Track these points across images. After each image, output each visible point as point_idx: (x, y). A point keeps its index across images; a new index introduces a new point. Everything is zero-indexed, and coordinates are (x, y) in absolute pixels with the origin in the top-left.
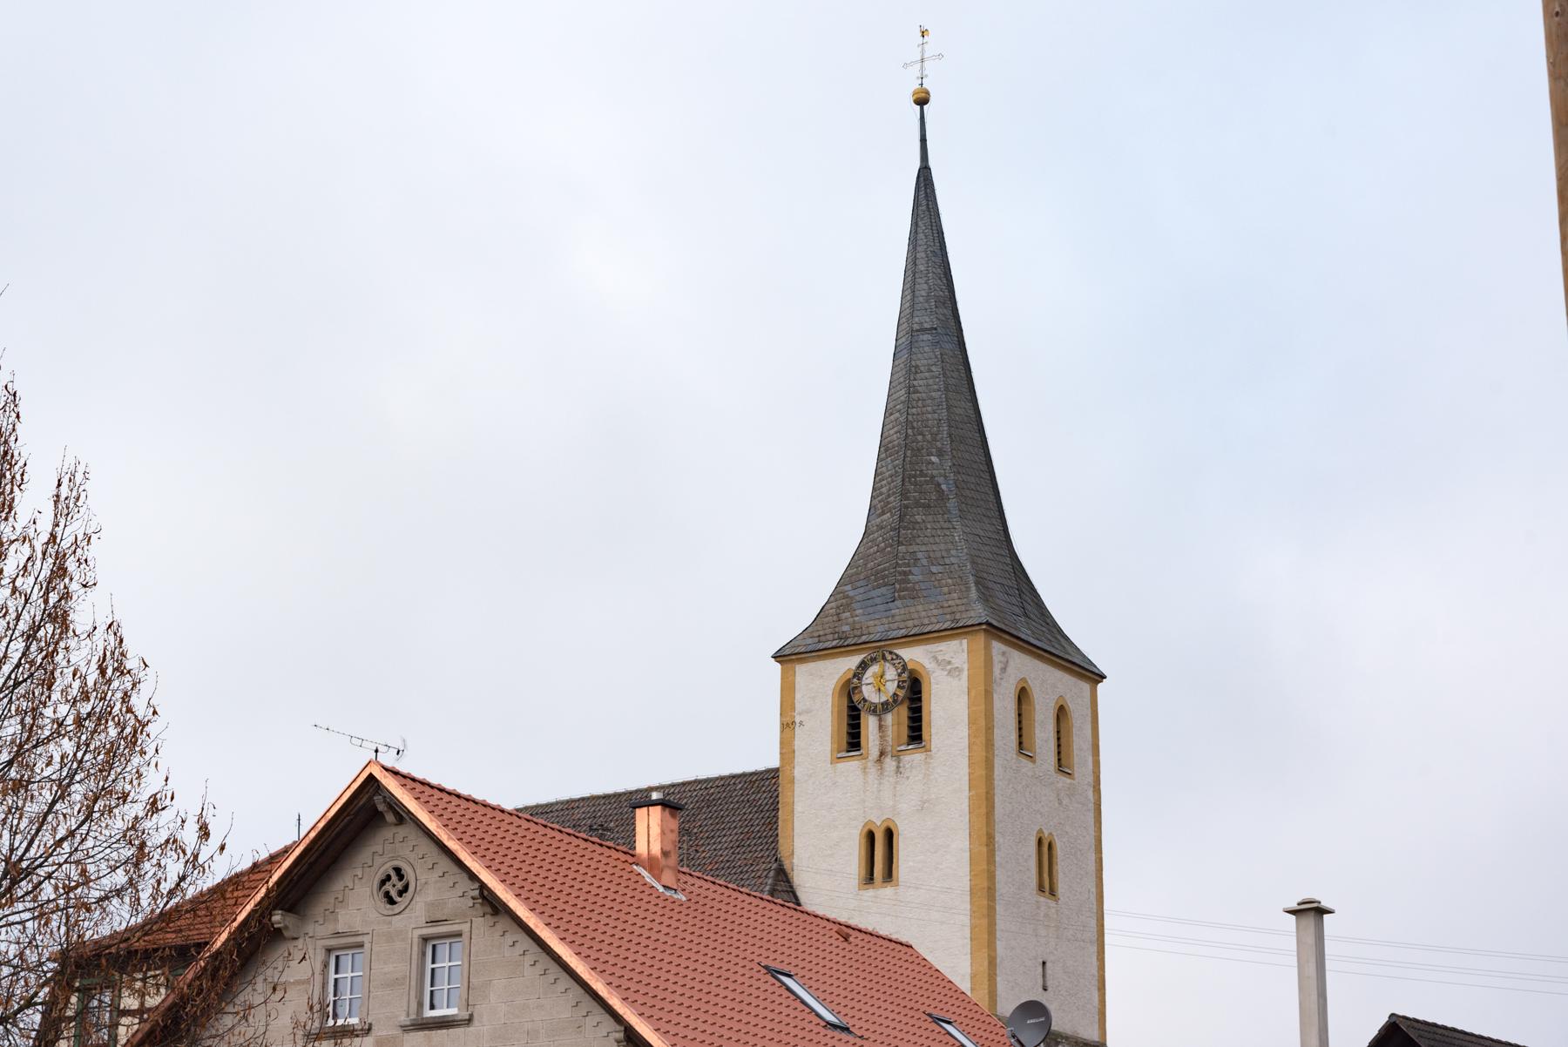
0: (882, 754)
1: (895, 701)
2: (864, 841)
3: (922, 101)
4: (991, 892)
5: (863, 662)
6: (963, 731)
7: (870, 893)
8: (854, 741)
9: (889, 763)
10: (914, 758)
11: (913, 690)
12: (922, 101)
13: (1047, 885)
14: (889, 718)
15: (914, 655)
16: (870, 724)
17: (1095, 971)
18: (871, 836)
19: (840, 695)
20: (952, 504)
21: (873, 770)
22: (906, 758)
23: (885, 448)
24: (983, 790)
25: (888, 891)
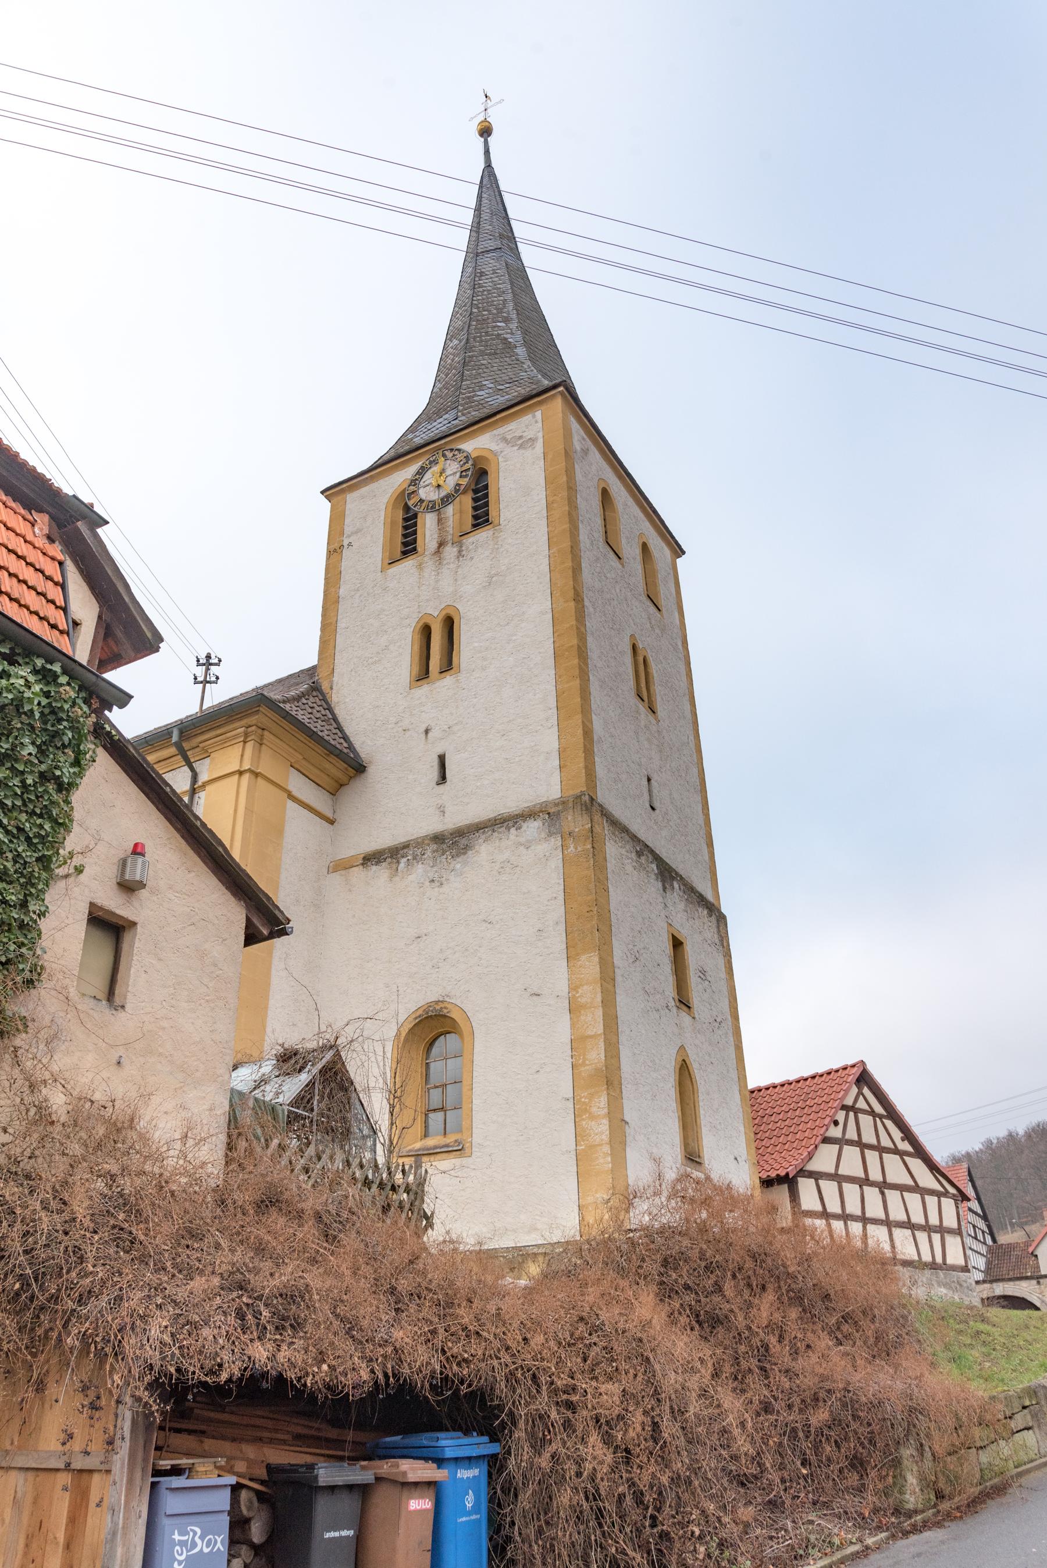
0: (441, 544)
1: (456, 491)
2: (417, 637)
3: (486, 131)
4: (582, 653)
5: (422, 468)
6: (539, 496)
7: (425, 689)
8: (409, 546)
9: (450, 551)
10: (483, 535)
11: (479, 486)
12: (486, 131)
13: (645, 694)
14: (450, 510)
15: (474, 445)
16: (428, 526)
17: (701, 822)
18: (426, 631)
19: (395, 506)
20: (521, 351)
21: (430, 564)
22: (469, 540)
23: (450, 336)
24: (567, 544)
25: (448, 680)
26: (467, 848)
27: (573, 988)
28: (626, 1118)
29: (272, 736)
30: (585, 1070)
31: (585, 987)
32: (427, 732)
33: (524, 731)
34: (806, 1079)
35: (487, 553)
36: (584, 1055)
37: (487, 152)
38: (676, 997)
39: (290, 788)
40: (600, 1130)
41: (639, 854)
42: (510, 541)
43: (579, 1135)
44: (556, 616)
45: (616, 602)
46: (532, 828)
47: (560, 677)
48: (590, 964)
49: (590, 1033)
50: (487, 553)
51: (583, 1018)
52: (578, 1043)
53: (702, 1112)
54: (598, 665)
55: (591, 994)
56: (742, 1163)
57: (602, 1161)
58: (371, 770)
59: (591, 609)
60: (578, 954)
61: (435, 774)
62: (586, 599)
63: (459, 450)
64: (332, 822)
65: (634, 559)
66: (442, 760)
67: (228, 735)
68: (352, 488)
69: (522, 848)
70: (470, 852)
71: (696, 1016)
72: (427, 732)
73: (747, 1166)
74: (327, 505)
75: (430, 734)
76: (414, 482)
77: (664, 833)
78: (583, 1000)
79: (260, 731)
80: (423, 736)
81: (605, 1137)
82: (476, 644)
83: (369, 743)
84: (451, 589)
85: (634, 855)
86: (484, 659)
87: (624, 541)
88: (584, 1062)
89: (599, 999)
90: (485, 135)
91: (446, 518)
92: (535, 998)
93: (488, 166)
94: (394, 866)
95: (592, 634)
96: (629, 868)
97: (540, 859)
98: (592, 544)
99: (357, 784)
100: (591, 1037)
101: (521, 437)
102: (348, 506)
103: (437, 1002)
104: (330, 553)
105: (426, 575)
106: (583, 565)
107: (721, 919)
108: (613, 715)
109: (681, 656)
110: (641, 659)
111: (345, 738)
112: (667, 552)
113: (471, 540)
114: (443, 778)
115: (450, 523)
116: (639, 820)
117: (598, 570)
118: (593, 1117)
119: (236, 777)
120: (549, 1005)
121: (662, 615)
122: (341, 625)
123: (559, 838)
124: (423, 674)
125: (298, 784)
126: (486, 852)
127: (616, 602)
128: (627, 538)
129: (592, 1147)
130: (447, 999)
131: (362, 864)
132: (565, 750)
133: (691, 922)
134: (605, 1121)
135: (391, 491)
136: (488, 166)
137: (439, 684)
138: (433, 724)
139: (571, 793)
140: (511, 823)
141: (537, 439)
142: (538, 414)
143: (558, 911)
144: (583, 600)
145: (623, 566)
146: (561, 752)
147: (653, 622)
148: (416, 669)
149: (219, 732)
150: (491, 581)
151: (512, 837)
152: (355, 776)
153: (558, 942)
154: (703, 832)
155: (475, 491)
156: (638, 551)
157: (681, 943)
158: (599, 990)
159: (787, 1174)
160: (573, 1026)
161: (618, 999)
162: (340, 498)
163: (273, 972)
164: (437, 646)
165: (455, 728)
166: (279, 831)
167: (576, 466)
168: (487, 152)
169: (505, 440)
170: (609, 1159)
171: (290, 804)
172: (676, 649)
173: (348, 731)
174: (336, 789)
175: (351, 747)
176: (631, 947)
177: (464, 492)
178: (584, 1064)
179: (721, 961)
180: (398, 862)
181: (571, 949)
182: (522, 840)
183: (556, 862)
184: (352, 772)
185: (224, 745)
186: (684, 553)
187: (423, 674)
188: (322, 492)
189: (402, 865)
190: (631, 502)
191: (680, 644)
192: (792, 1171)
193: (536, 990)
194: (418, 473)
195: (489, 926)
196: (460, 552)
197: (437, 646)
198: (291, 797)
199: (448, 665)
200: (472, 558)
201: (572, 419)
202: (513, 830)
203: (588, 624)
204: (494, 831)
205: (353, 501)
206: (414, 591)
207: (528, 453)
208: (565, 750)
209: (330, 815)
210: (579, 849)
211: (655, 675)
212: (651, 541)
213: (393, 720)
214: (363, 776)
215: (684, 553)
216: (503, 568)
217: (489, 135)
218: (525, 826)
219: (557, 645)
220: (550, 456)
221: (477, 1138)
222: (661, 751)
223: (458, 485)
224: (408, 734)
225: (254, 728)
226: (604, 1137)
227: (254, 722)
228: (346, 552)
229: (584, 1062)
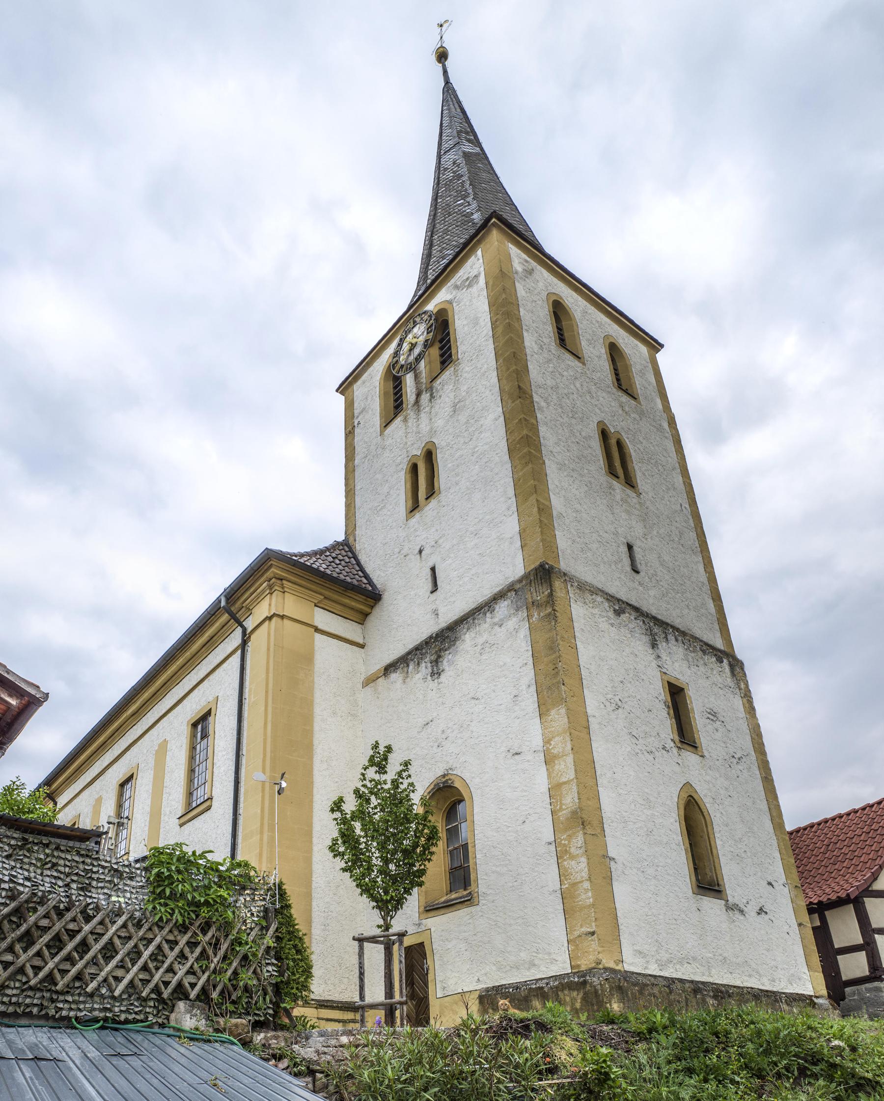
0: (418, 395)
2: (409, 476)
3: (442, 56)
5: (401, 339)
9: (425, 397)
12: (442, 56)
18: (414, 468)
21: (411, 414)
25: (433, 502)
26: (456, 639)
27: (547, 741)
28: (611, 854)
29: (290, 584)
30: (563, 814)
31: (557, 739)
32: (420, 552)
33: (491, 525)
34: (872, 806)
35: (451, 387)
36: (561, 800)
37: (445, 72)
38: (677, 738)
39: (316, 624)
40: (579, 867)
41: (618, 613)
42: (467, 369)
43: (563, 875)
44: (507, 416)
45: (575, 396)
46: (503, 608)
47: (515, 467)
48: (559, 717)
49: (564, 779)
50: (451, 387)
51: (557, 767)
52: (555, 791)
53: (718, 842)
54: (554, 450)
55: (562, 745)
56: (778, 886)
57: (583, 897)
58: (385, 597)
59: (543, 404)
60: (548, 710)
61: (429, 586)
62: (534, 395)
63: (425, 313)
64: (362, 646)
65: (599, 357)
66: (433, 569)
67: (258, 591)
68: (356, 379)
69: (496, 627)
70: (458, 643)
71: (706, 753)
72: (420, 552)
73: (786, 890)
74: (342, 398)
75: (423, 553)
76: (396, 354)
77: (652, 593)
78: (555, 751)
79: (279, 582)
80: (418, 556)
81: (585, 874)
82: (450, 465)
83: (383, 575)
84: (428, 428)
85: (611, 614)
86: (457, 475)
87: (584, 343)
88: (561, 807)
89: (569, 747)
90: (443, 59)
91: (420, 372)
92: (516, 757)
93: (447, 82)
94: (405, 669)
95: (546, 424)
96: (604, 625)
97: (511, 633)
98: (541, 348)
99: (376, 612)
100: (565, 783)
101: (468, 279)
102: (355, 394)
103: (444, 776)
104: (347, 435)
105: (410, 424)
106: (530, 367)
107: (736, 666)
108: (577, 492)
109: (669, 435)
110: (613, 442)
111: (366, 576)
112: (643, 349)
113: (438, 382)
114: (435, 588)
115: (424, 375)
116: (617, 583)
117: (550, 369)
118: (572, 857)
119: (267, 622)
120: (528, 761)
121: (640, 404)
122: (358, 488)
123: (525, 611)
124: (415, 506)
125: (323, 619)
126: (468, 640)
127: (575, 396)
128: (588, 340)
129: (574, 885)
130: (450, 772)
131: (384, 674)
132: (524, 530)
133: (695, 669)
134: (584, 860)
135: (382, 369)
136: (447, 82)
137: (427, 508)
138: (424, 544)
139: (533, 567)
140: (486, 608)
141: (480, 274)
142: (479, 252)
143: (528, 674)
144: (532, 397)
145: (584, 364)
146: (522, 533)
147: (627, 409)
148: (410, 503)
149: (252, 590)
150: (455, 409)
151: (488, 620)
152: (375, 604)
153: (530, 701)
154: (707, 588)
155: (441, 341)
156: (603, 351)
157: (682, 690)
158: (568, 739)
159: (848, 895)
160: (549, 776)
161: (594, 745)
162: (350, 390)
163: (316, 772)
164: (423, 477)
165: (441, 541)
166: (308, 658)
167: (517, 284)
168: (445, 72)
169: (457, 287)
170: (590, 894)
171: (318, 636)
172: (660, 429)
173: (369, 570)
174: (362, 618)
175: (370, 582)
176: (609, 696)
177: (432, 345)
178: (561, 809)
179: (738, 703)
180: (408, 666)
181: (542, 707)
182: (496, 620)
183: (524, 631)
184: (371, 602)
185: (258, 600)
186: (662, 346)
187: (415, 506)
188: (337, 391)
189: (411, 667)
190: (591, 309)
191: (665, 425)
192: (853, 892)
193: (517, 750)
194: (399, 345)
195: (477, 702)
196: (431, 395)
197: (423, 477)
198: (317, 630)
199: (432, 492)
200: (440, 396)
201: (510, 245)
202: (488, 615)
203: (539, 415)
204: (474, 619)
205: (359, 389)
206: (404, 440)
207: (474, 290)
208: (524, 530)
209: (361, 642)
210: (542, 614)
211: (633, 454)
212: (621, 341)
213: (397, 550)
214: (380, 603)
215: (662, 346)
216: (464, 394)
217: (446, 58)
218: (497, 607)
219: (510, 441)
220: (491, 283)
221: (482, 889)
222: (644, 520)
223: (427, 341)
224: (408, 558)
225: (273, 580)
226: (584, 874)
227: (272, 575)
228: (357, 431)
229: (561, 807)
